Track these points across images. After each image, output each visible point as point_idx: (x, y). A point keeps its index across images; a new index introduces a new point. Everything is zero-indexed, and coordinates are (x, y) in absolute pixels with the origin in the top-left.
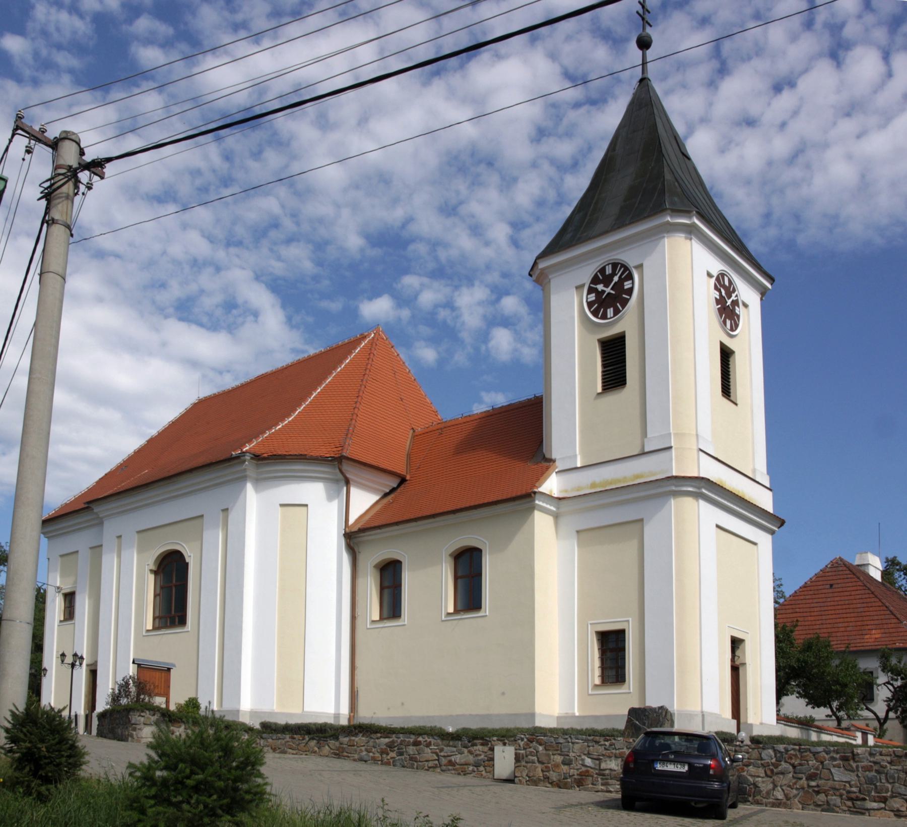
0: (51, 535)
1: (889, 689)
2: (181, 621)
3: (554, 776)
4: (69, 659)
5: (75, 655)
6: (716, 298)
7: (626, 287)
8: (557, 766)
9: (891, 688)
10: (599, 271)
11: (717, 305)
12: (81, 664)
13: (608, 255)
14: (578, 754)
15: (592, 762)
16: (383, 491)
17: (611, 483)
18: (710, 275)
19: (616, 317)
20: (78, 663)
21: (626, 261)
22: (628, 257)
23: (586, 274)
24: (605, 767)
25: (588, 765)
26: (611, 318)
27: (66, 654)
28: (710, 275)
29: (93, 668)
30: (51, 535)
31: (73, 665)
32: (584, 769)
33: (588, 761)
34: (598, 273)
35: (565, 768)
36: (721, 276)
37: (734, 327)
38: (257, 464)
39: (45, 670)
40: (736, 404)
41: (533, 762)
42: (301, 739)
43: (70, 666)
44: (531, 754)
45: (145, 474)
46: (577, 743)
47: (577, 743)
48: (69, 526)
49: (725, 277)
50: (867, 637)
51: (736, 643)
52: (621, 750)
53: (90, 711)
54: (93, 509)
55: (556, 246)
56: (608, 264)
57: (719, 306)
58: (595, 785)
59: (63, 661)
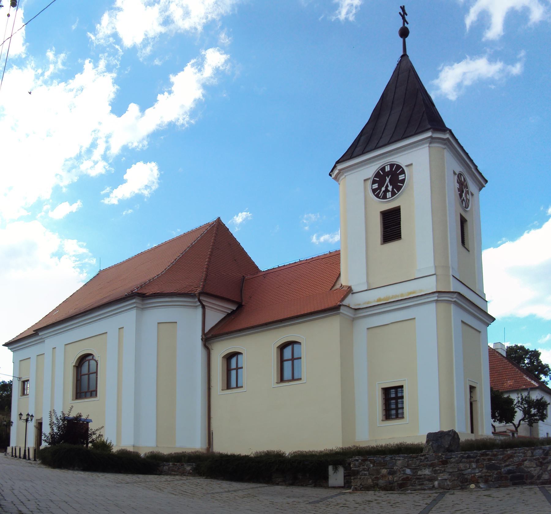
0: (15, 350)
1: (519, 409)
2: (386, 391)
3: (381, 482)
4: (24, 417)
5: (28, 415)
6: (458, 188)
7: (400, 179)
8: (383, 476)
9: (520, 408)
10: (381, 170)
11: (459, 192)
12: (32, 420)
13: (385, 160)
14: (400, 467)
15: (411, 471)
16: (228, 312)
17: (392, 298)
18: (455, 173)
19: (399, 193)
20: (30, 419)
21: (400, 162)
22: (401, 160)
23: (371, 171)
24: (421, 474)
25: (408, 474)
26: (389, 198)
27: (22, 414)
28: (455, 173)
29: (40, 421)
30: (15, 350)
31: (27, 420)
32: (405, 476)
33: (408, 471)
34: (380, 171)
35: (390, 477)
36: (460, 175)
37: (467, 207)
38: (142, 300)
39: (12, 422)
40: (469, 251)
41: (365, 475)
42: (180, 465)
43: (25, 421)
44: (364, 470)
45: (71, 311)
46: (399, 460)
47: (399, 460)
48: (25, 344)
49: (462, 176)
50: (505, 384)
51: (472, 388)
52: (432, 462)
53: (37, 445)
54: (39, 334)
55: (350, 154)
56: (387, 165)
57: (459, 192)
58: (413, 486)
59: (20, 418)
